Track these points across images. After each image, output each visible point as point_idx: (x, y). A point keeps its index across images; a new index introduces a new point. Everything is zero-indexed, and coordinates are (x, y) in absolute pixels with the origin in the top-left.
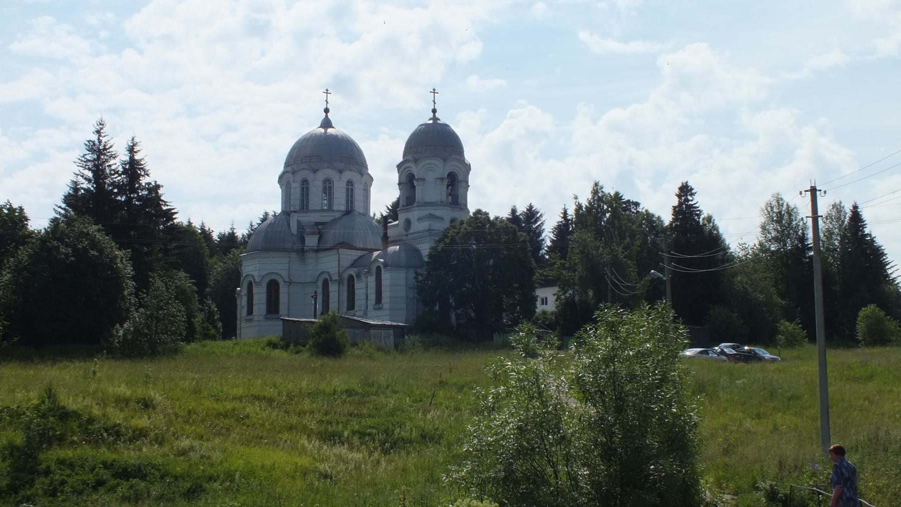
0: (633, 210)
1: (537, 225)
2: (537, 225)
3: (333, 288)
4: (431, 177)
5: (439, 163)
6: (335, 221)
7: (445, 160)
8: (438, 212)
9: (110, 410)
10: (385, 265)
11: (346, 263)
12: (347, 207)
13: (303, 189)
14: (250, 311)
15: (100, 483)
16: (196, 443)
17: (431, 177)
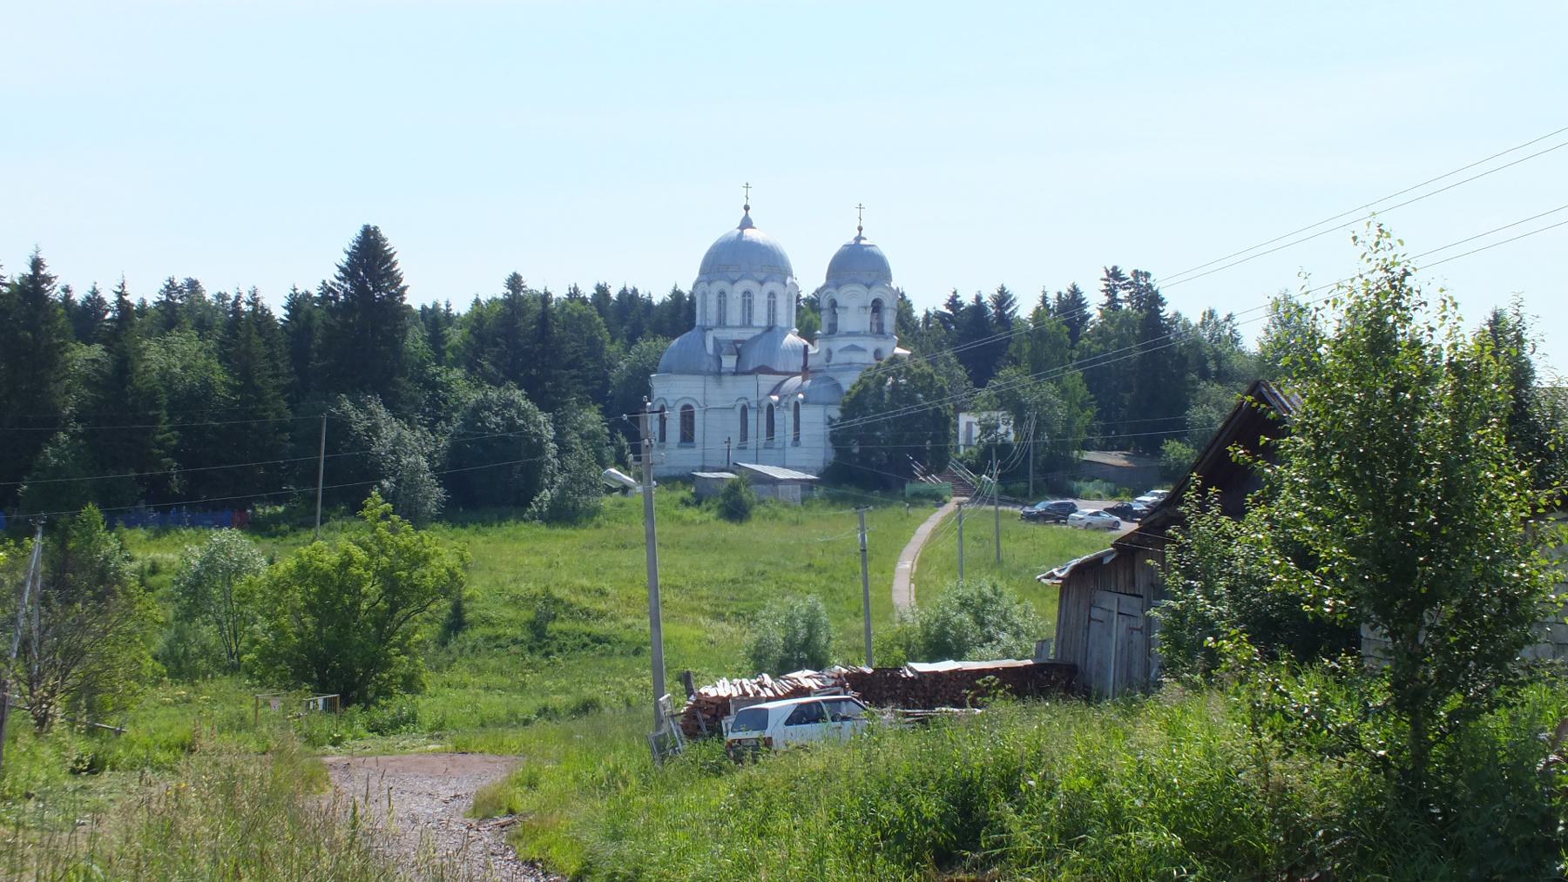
0: (1141, 283)
1: (1009, 311)
2: (1009, 311)
3: (751, 416)
4: (854, 304)
5: (859, 289)
6: (755, 339)
7: (869, 286)
8: (859, 342)
9: (582, 598)
10: (805, 401)
11: (765, 389)
12: (769, 323)
13: (720, 302)
14: (663, 438)
15: (585, 645)
16: (636, 621)
17: (854, 304)
